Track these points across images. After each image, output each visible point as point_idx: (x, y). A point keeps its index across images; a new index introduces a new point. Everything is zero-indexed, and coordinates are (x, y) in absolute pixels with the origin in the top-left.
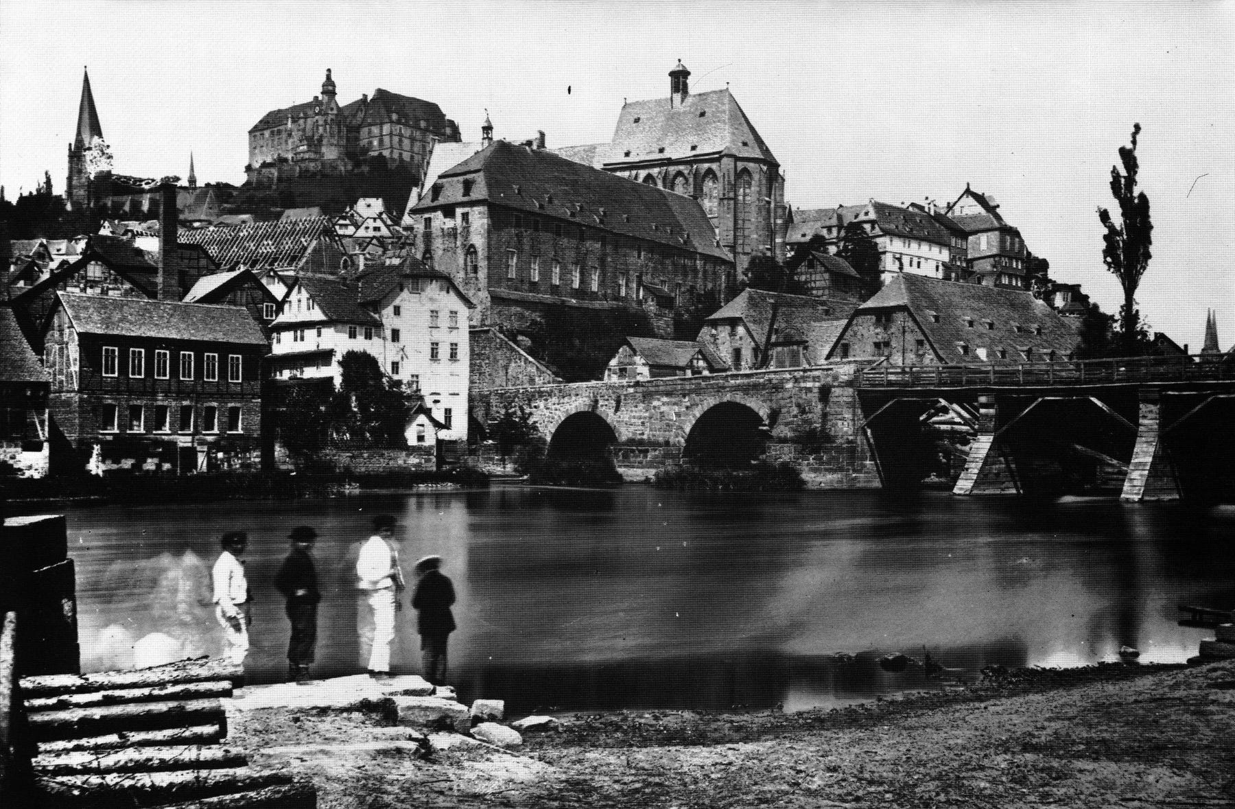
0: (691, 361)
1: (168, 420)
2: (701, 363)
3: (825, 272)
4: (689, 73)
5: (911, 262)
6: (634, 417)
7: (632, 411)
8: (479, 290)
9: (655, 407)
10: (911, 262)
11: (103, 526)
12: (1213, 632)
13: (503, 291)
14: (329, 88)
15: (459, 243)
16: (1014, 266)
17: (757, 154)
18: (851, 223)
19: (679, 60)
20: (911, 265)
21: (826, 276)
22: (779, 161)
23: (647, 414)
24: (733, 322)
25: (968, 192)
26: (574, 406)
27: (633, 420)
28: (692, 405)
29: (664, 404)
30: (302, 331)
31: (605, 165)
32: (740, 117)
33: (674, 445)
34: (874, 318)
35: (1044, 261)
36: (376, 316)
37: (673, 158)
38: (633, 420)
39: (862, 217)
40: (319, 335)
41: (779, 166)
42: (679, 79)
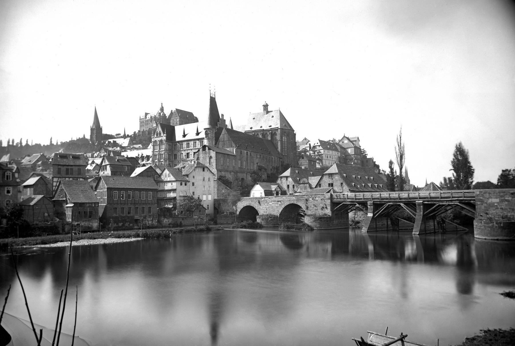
0: (276, 189)
1: (398, 204)
4: (268, 105)
5: (330, 157)
7: (263, 206)
8: (213, 169)
10: (330, 157)
11: (470, 208)
14: (162, 109)
16: (358, 157)
18: (313, 146)
24: (287, 177)
26: (245, 204)
27: (263, 208)
28: (281, 204)
29: (273, 204)
30: (167, 183)
32: (282, 118)
33: (58, 230)
35: (225, 120)
36: (188, 179)
39: (316, 145)
41: (294, 131)
42: (266, 107)
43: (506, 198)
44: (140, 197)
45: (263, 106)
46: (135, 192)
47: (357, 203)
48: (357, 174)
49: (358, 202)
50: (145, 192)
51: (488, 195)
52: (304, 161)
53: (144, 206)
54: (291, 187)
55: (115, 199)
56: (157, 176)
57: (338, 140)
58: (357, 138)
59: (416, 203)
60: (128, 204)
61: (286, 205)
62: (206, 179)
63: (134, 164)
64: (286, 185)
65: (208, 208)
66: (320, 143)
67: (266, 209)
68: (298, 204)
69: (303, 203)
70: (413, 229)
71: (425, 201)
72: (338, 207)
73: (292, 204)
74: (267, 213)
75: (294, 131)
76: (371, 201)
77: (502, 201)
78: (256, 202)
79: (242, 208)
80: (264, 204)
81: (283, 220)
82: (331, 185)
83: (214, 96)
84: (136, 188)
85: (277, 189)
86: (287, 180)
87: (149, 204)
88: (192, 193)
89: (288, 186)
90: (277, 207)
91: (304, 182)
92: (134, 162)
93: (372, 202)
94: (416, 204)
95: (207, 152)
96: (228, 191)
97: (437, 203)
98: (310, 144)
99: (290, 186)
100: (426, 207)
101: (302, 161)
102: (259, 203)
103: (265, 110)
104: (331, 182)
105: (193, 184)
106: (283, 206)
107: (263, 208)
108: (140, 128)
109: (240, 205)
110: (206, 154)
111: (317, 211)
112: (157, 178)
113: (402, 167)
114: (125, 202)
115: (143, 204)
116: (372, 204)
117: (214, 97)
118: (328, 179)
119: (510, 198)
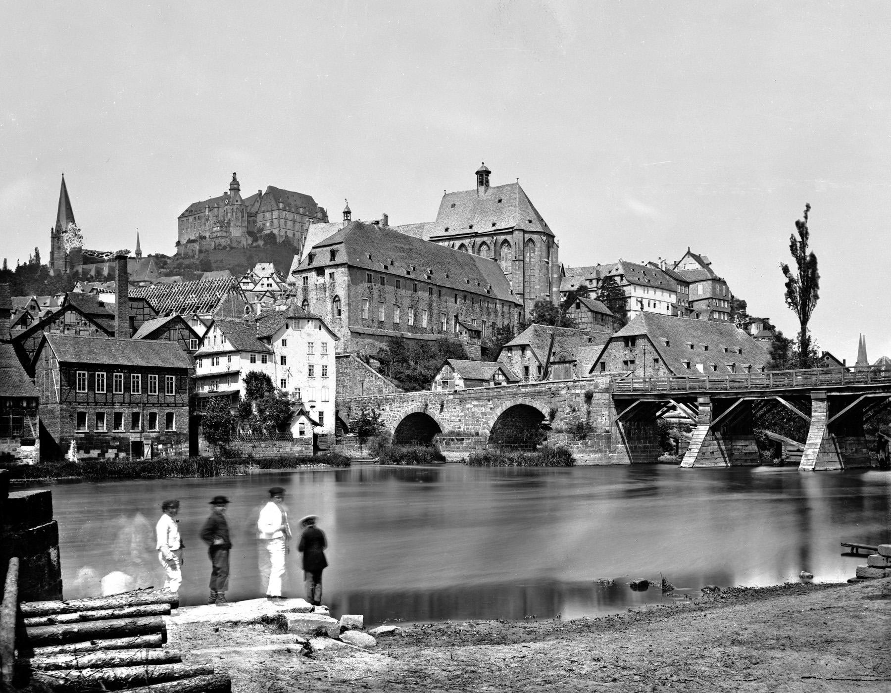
2: (501, 377)
3: (588, 312)
4: (490, 172)
6: (454, 416)
7: (452, 412)
8: (342, 327)
14: (235, 186)
15: (327, 294)
17: (539, 228)
19: (483, 163)
21: (589, 314)
24: (523, 348)
25: (689, 253)
27: (452, 418)
29: (474, 406)
31: (431, 238)
34: (623, 343)
36: (270, 347)
38: (452, 418)
39: (614, 273)
40: (229, 360)
41: (554, 237)
42: (483, 176)
44: (145, 386)
45: (477, 173)
46: (132, 375)
48: (698, 337)
49: (674, 397)
50: (157, 376)
52: (580, 315)
53: (156, 411)
55: (80, 392)
56: (196, 341)
57: (673, 263)
60: (113, 405)
61: (505, 409)
63: (144, 315)
64: (522, 367)
66: (624, 269)
67: (460, 420)
68: (534, 406)
70: (802, 456)
72: (628, 409)
73: (521, 405)
75: (554, 237)
78: (435, 404)
79: (403, 418)
80: (455, 408)
84: (135, 364)
85: (496, 376)
87: (168, 404)
88: (280, 382)
89: (527, 368)
90: (484, 414)
91: (562, 359)
92: (143, 308)
95: (327, 286)
96: (378, 383)
97: (861, 393)
99: (530, 369)
101: (576, 314)
102: (442, 406)
103: (482, 185)
104: (628, 358)
105: (283, 360)
106: (499, 412)
107: (450, 416)
108: (180, 236)
109: (398, 411)
110: (325, 291)
112: (195, 345)
113: (808, 320)
114: (124, 400)
115: (153, 404)
118: (622, 351)
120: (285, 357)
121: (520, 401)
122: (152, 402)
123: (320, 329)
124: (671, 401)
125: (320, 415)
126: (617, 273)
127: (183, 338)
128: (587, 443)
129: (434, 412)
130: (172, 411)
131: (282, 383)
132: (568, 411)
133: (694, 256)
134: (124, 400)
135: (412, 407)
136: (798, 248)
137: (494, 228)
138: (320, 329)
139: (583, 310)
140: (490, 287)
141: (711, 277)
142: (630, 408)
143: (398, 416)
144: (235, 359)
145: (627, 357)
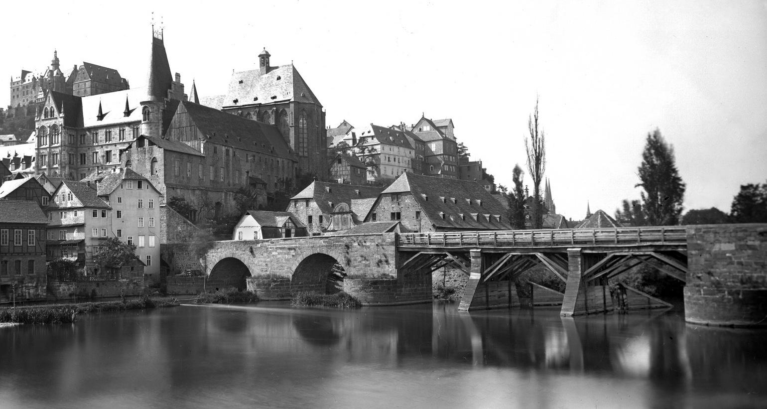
0: (285, 224)
2: (291, 225)
4: (270, 55)
5: (395, 159)
8: (159, 183)
9: (274, 255)
10: (395, 159)
12: (558, 359)
13: (173, 181)
15: (147, 156)
19: (264, 48)
20: (395, 161)
22: (322, 104)
23: (268, 260)
24: (307, 200)
25: (423, 118)
29: (279, 254)
31: (223, 107)
36: (108, 203)
37: (262, 103)
39: (366, 134)
40: (76, 215)
42: (265, 58)
43: (750, 243)
47: (448, 252)
51: (712, 235)
52: (341, 169)
53: (20, 259)
54: (316, 220)
58: (449, 121)
59: (568, 253)
62: (145, 204)
65: (149, 262)
67: (266, 265)
69: (339, 251)
70: (561, 304)
71: (585, 248)
72: (410, 260)
73: (319, 254)
74: (268, 273)
76: (477, 248)
77: (740, 248)
78: (244, 251)
80: (262, 255)
81: (299, 287)
82: (397, 216)
83: (160, 37)
85: (287, 224)
86: (307, 205)
90: (288, 260)
93: (479, 250)
94: (567, 254)
98: (354, 134)
99: (314, 218)
100: (589, 259)
105: (119, 214)
107: (259, 261)
110: (145, 154)
111: (369, 268)
115: (18, 253)
116: (480, 254)
117: (161, 39)
119: (757, 243)
120: (120, 212)
121: (318, 251)
122: (17, 252)
123: (148, 188)
124: (449, 254)
125: (148, 258)
126: (369, 135)
127: (37, 196)
128: (378, 287)
129: (244, 257)
130: (33, 259)
131: (118, 233)
132: (360, 260)
133: (427, 120)
134: (14, 251)
135: (225, 252)
136: (535, 135)
137: (275, 100)
138: (148, 188)
139: (344, 165)
140: (273, 148)
141: (441, 138)
142: (413, 257)
143: (213, 260)
144: (81, 214)
145: (395, 209)
